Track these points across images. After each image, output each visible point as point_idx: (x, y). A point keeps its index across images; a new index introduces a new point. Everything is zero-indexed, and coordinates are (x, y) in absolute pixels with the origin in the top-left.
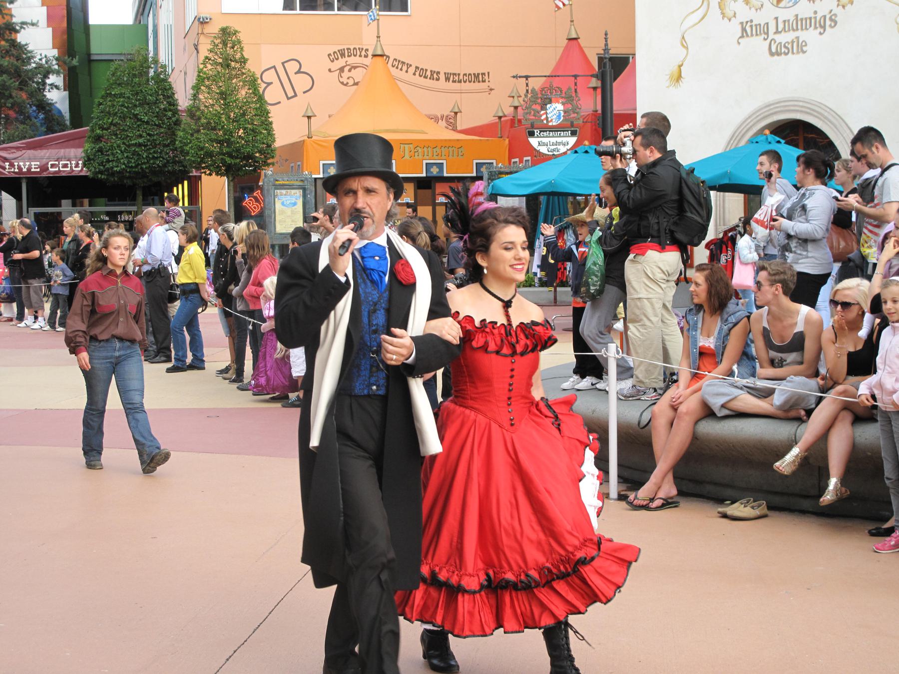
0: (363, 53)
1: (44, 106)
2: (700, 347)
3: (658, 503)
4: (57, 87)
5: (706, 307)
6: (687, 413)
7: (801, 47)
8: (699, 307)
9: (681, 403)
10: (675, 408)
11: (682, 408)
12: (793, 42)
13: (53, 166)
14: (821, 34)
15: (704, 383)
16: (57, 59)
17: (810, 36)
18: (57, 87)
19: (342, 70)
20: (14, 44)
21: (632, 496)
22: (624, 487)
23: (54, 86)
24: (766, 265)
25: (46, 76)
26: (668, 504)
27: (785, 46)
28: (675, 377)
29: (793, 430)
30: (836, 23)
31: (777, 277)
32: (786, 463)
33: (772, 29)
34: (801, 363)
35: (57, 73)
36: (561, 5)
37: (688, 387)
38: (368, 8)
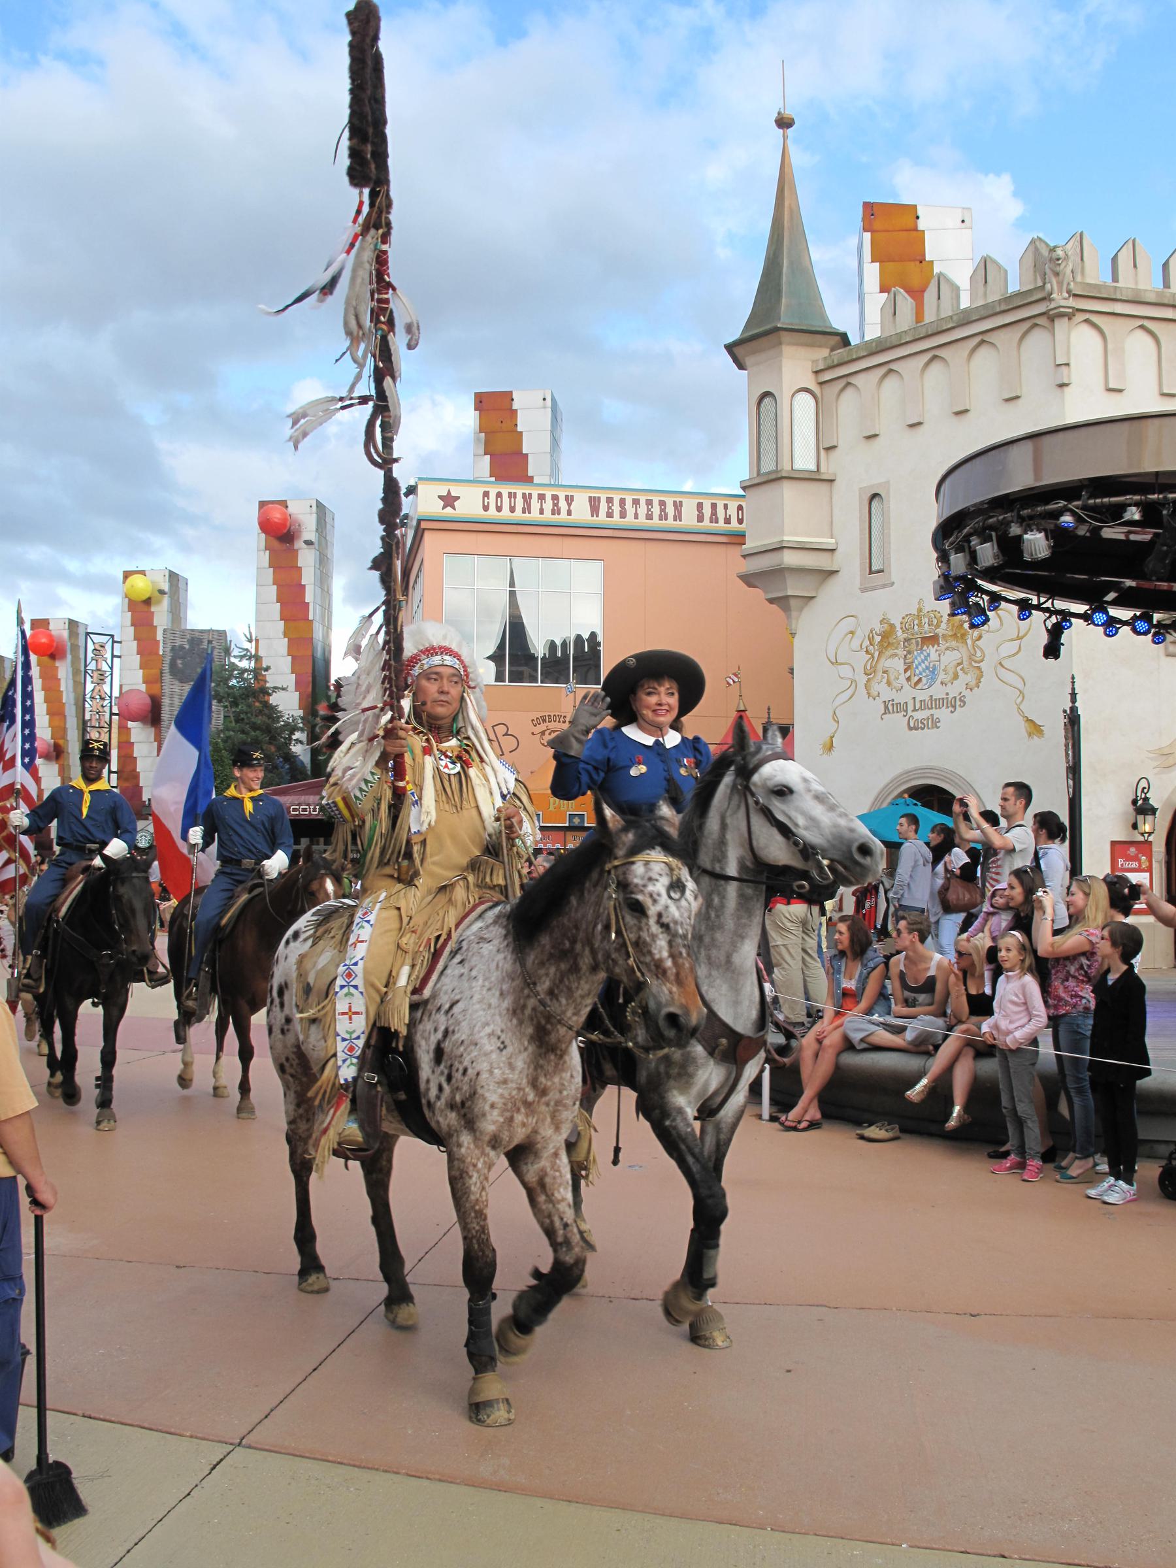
0: (562, 719)
1: (290, 758)
2: (844, 989)
3: (804, 1125)
4: (301, 742)
5: (849, 954)
6: (830, 1046)
7: (935, 723)
8: (842, 954)
9: (825, 1037)
10: (819, 1042)
11: (826, 1042)
12: (928, 719)
13: (294, 810)
14: (952, 712)
15: (846, 1019)
16: (302, 718)
17: (943, 714)
18: (301, 742)
19: (543, 733)
20: (266, 705)
21: (783, 1118)
22: (775, 1109)
23: (298, 741)
24: (906, 915)
25: (292, 733)
26: (813, 1125)
27: (922, 723)
28: (820, 1014)
29: (923, 1063)
30: (965, 703)
31: (915, 927)
32: (916, 1092)
33: (910, 708)
34: (931, 1004)
35: (302, 730)
36: (732, 682)
37: (832, 1023)
38: (567, 681)
